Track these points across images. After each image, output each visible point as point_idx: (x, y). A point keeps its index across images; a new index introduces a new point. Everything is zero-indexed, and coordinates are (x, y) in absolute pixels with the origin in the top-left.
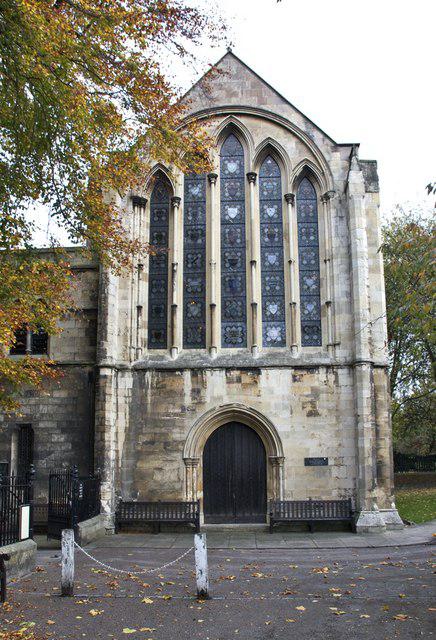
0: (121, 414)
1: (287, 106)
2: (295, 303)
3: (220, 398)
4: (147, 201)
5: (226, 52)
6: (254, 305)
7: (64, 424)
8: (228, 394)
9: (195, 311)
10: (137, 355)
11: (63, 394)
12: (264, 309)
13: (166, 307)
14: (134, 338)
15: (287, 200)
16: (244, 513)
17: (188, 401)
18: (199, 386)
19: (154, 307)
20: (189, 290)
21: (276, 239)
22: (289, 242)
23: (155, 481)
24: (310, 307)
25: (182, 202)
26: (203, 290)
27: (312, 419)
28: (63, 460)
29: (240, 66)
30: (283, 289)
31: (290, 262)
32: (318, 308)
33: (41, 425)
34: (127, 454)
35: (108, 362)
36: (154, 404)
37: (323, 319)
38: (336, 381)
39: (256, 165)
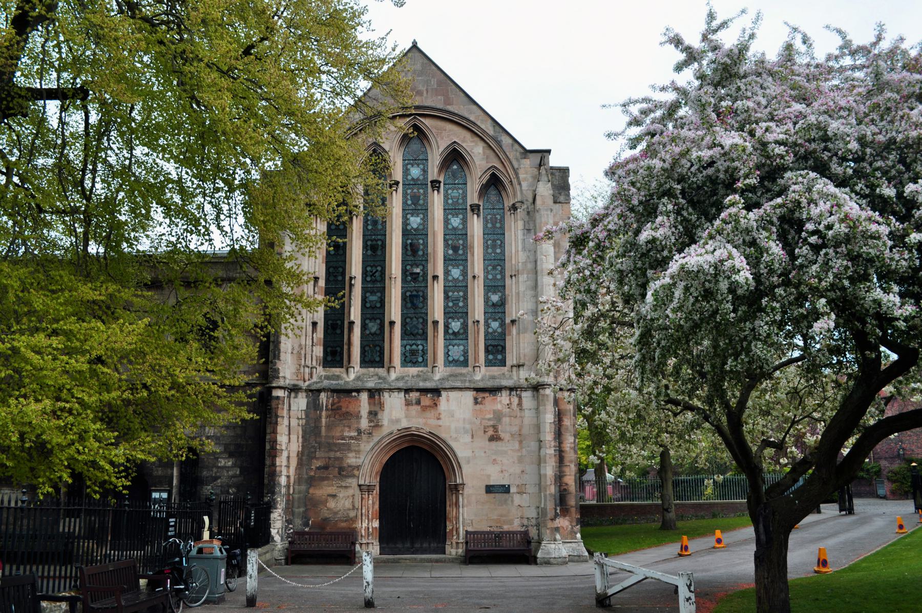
0: (294, 437)
2: (478, 322)
3: (398, 421)
5: (410, 45)
7: (232, 448)
8: (406, 417)
9: (373, 327)
12: (447, 327)
15: (473, 210)
16: (845, 173)
17: (364, 423)
18: (377, 409)
20: (368, 305)
21: (461, 252)
22: (473, 255)
23: (328, 509)
27: (494, 444)
28: (229, 486)
30: (466, 305)
32: (503, 324)
34: (299, 480)
35: (281, 383)
36: (329, 427)
37: (508, 338)
38: (520, 404)
39: (440, 171)
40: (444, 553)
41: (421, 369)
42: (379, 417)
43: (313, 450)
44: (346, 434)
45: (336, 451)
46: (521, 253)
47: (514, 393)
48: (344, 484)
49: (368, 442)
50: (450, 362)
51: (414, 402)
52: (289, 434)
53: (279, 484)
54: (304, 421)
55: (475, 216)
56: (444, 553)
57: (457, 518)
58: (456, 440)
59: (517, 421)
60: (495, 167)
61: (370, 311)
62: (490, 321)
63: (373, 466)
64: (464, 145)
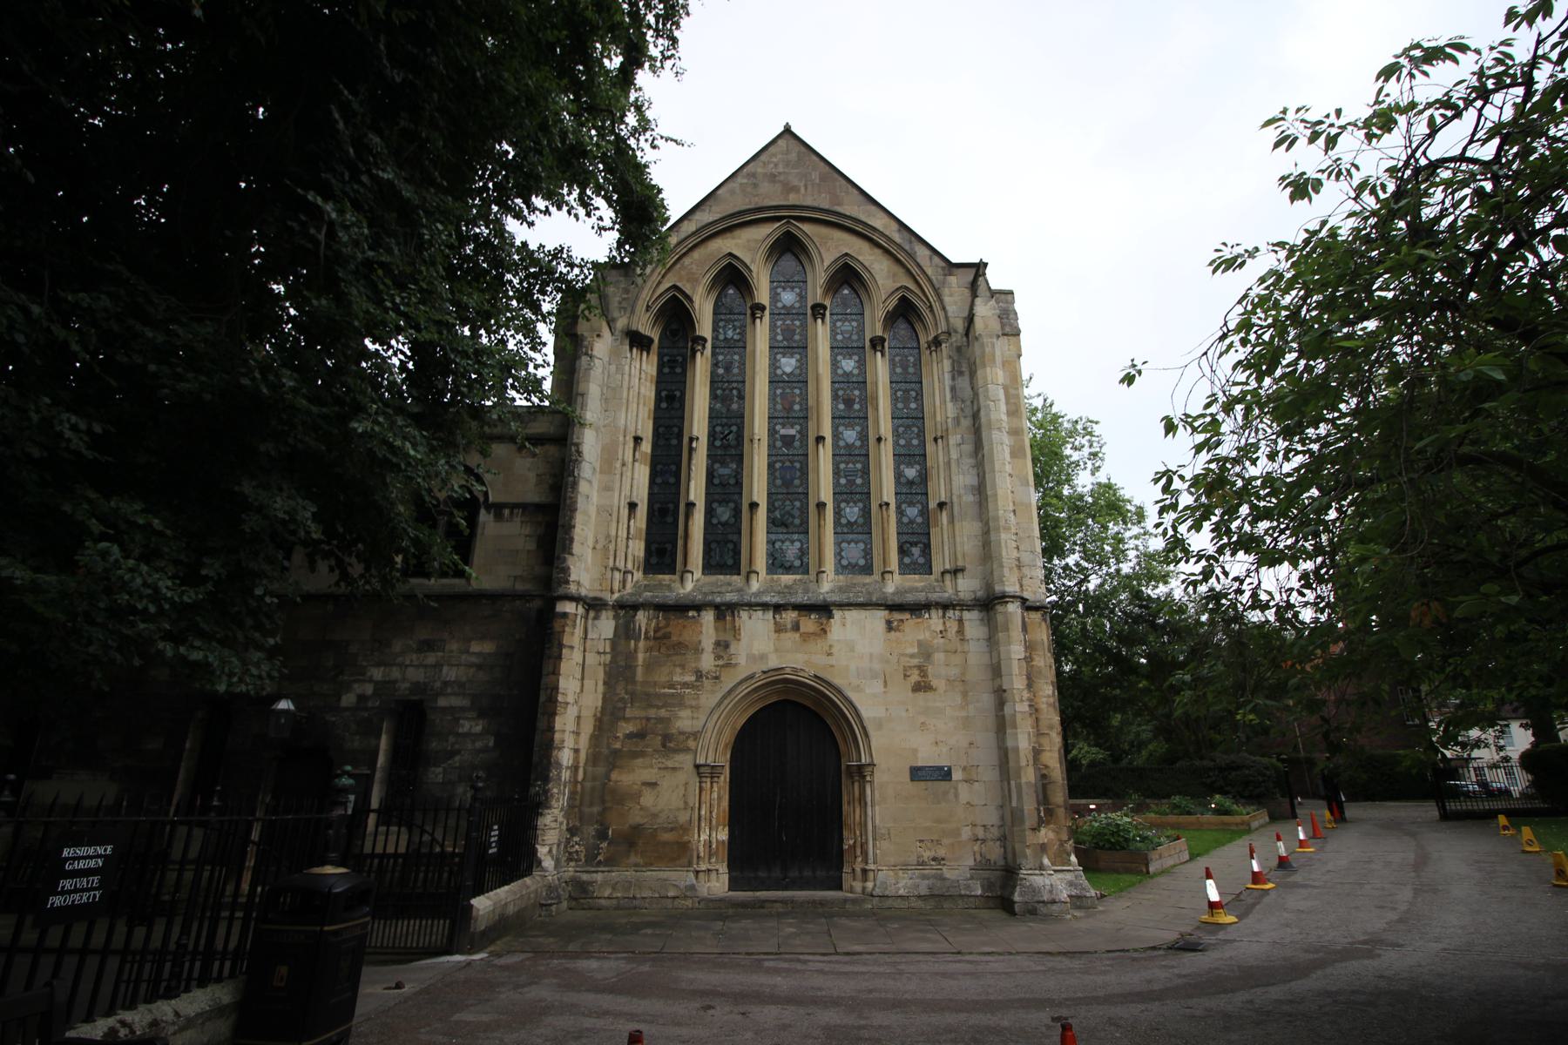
0: (589, 683)
1: (873, 208)
2: (887, 504)
3: (763, 657)
4: (651, 341)
5: (782, 129)
6: (821, 506)
8: (776, 650)
9: (724, 514)
10: (624, 582)
11: (487, 647)
12: (838, 513)
13: (677, 507)
14: (621, 555)
17: (707, 662)
18: (728, 637)
19: (657, 506)
20: (716, 481)
21: (857, 407)
22: (877, 409)
24: (912, 512)
25: (709, 345)
26: (739, 484)
27: (921, 695)
29: (803, 149)
31: (879, 440)
32: (925, 512)
33: (442, 702)
34: (594, 759)
35: (573, 589)
36: (649, 667)
37: (933, 531)
38: (961, 631)
40: (840, 888)
41: (798, 577)
42: (732, 649)
43: (620, 705)
44: (677, 678)
45: (659, 708)
46: (950, 405)
47: (950, 613)
48: (670, 764)
49: (713, 692)
50: (844, 567)
51: (789, 626)
52: (583, 679)
53: (559, 765)
54: (608, 657)
55: (879, 354)
56: (840, 888)
57: (864, 825)
58: (858, 689)
59: (957, 659)
60: (906, 288)
61: (719, 490)
62: (904, 506)
63: (720, 733)
64: (860, 258)
